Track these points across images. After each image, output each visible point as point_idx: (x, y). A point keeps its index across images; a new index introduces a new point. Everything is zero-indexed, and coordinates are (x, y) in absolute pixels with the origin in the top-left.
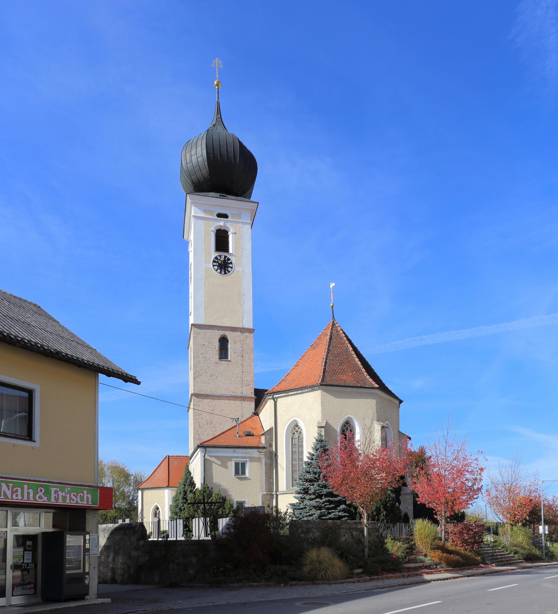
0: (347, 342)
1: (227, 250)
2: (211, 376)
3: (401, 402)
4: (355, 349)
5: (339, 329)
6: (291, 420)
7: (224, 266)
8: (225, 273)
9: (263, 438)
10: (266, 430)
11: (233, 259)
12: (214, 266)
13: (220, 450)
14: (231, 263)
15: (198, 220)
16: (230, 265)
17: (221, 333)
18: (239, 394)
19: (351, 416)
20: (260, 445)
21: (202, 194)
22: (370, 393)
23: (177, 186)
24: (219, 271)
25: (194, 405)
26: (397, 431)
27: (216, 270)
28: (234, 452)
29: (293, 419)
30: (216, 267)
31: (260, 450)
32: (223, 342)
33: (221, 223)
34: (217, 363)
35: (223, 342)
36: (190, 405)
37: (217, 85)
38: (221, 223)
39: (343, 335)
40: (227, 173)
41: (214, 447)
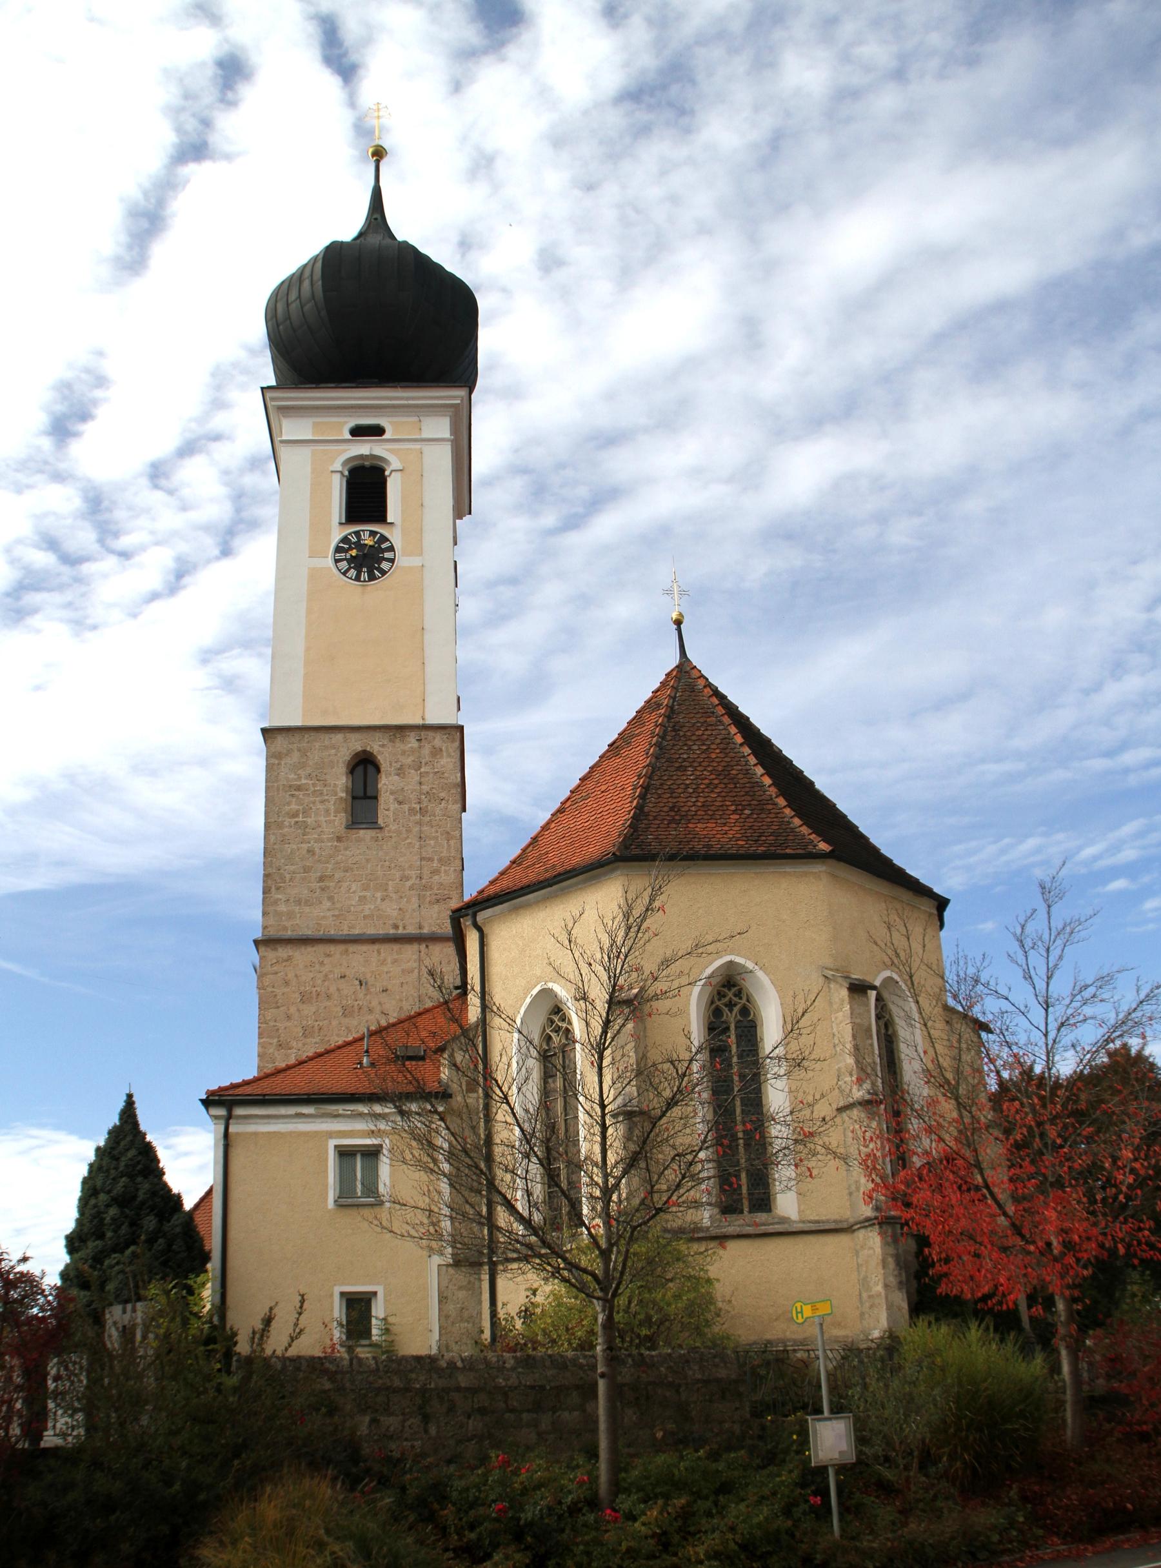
0: (727, 720)
2: (321, 879)
6: (535, 992)
8: (372, 578)
11: (395, 537)
12: (337, 561)
14: (391, 549)
16: (387, 555)
17: (356, 744)
18: (412, 930)
19: (740, 960)
27: (344, 574)
29: (538, 988)
30: (344, 565)
33: (365, 448)
38: (365, 448)
39: (715, 701)
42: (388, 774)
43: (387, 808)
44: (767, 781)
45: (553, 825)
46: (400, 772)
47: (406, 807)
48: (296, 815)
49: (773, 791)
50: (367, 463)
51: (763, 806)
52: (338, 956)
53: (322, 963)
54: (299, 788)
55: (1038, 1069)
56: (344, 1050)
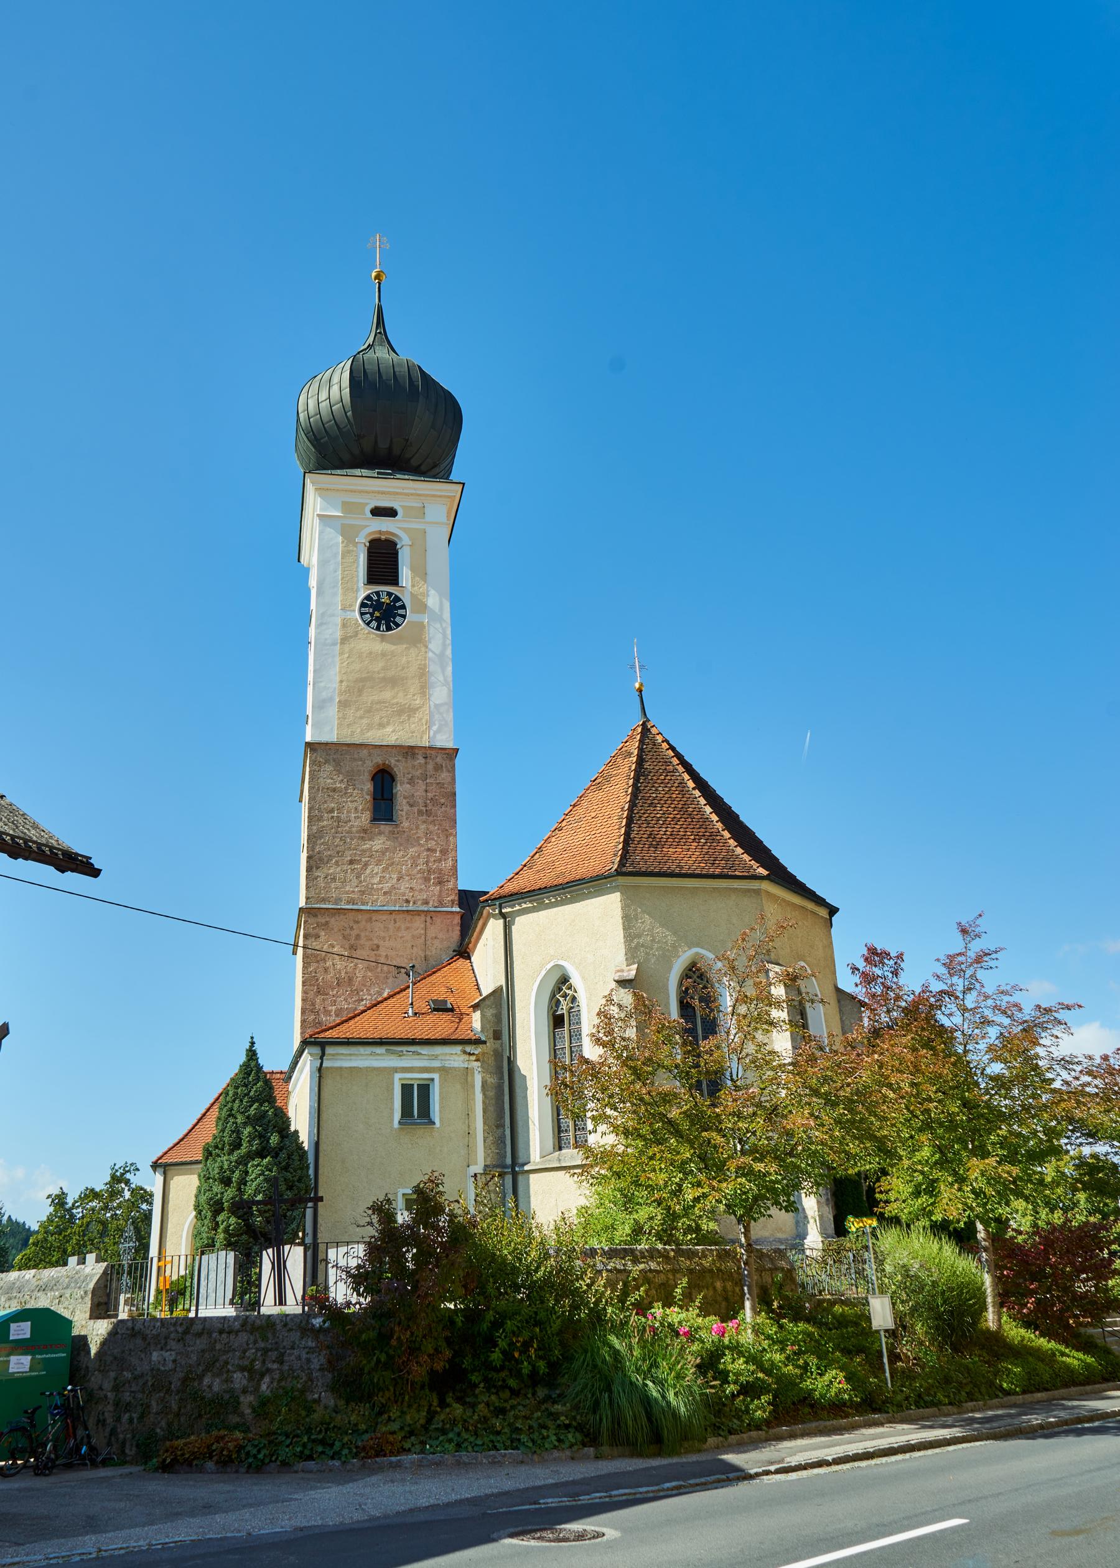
0: (681, 769)
1: (395, 581)
2: (351, 862)
3: (833, 911)
4: (702, 785)
5: (659, 739)
6: (549, 967)
7: (384, 614)
8: (389, 629)
9: (477, 1016)
10: (486, 992)
12: (362, 614)
13: (362, 1050)
14: (403, 607)
15: (328, 520)
16: (401, 612)
20: (471, 1036)
21: (339, 472)
22: (749, 890)
23: (288, 455)
24: (374, 624)
25: (306, 937)
26: (832, 988)
27: (368, 624)
28: (400, 1055)
29: (552, 964)
31: (468, 1049)
32: (383, 783)
33: (384, 525)
34: (365, 831)
35: (383, 783)
36: (297, 937)
37: (378, 277)
38: (384, 525)
39: (671, 753)
40: (394, 426)
41: (348, 1043)
42: (402, 783)
43: (401, 806)
44: (714, 818)
45: (553, 839)
46: (411, 781)
47: (415, 809)
48: (332, 811)
49: (720, 826)
50: (383, 537)
51: (713, 836)
52: (364, 923)
53: (352, 928)
54: (334, 790)
55: (329, 768)
56: (389, 1002)
